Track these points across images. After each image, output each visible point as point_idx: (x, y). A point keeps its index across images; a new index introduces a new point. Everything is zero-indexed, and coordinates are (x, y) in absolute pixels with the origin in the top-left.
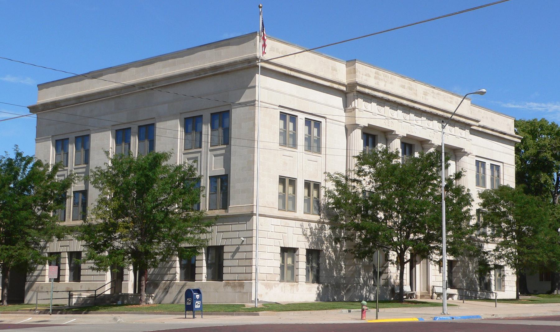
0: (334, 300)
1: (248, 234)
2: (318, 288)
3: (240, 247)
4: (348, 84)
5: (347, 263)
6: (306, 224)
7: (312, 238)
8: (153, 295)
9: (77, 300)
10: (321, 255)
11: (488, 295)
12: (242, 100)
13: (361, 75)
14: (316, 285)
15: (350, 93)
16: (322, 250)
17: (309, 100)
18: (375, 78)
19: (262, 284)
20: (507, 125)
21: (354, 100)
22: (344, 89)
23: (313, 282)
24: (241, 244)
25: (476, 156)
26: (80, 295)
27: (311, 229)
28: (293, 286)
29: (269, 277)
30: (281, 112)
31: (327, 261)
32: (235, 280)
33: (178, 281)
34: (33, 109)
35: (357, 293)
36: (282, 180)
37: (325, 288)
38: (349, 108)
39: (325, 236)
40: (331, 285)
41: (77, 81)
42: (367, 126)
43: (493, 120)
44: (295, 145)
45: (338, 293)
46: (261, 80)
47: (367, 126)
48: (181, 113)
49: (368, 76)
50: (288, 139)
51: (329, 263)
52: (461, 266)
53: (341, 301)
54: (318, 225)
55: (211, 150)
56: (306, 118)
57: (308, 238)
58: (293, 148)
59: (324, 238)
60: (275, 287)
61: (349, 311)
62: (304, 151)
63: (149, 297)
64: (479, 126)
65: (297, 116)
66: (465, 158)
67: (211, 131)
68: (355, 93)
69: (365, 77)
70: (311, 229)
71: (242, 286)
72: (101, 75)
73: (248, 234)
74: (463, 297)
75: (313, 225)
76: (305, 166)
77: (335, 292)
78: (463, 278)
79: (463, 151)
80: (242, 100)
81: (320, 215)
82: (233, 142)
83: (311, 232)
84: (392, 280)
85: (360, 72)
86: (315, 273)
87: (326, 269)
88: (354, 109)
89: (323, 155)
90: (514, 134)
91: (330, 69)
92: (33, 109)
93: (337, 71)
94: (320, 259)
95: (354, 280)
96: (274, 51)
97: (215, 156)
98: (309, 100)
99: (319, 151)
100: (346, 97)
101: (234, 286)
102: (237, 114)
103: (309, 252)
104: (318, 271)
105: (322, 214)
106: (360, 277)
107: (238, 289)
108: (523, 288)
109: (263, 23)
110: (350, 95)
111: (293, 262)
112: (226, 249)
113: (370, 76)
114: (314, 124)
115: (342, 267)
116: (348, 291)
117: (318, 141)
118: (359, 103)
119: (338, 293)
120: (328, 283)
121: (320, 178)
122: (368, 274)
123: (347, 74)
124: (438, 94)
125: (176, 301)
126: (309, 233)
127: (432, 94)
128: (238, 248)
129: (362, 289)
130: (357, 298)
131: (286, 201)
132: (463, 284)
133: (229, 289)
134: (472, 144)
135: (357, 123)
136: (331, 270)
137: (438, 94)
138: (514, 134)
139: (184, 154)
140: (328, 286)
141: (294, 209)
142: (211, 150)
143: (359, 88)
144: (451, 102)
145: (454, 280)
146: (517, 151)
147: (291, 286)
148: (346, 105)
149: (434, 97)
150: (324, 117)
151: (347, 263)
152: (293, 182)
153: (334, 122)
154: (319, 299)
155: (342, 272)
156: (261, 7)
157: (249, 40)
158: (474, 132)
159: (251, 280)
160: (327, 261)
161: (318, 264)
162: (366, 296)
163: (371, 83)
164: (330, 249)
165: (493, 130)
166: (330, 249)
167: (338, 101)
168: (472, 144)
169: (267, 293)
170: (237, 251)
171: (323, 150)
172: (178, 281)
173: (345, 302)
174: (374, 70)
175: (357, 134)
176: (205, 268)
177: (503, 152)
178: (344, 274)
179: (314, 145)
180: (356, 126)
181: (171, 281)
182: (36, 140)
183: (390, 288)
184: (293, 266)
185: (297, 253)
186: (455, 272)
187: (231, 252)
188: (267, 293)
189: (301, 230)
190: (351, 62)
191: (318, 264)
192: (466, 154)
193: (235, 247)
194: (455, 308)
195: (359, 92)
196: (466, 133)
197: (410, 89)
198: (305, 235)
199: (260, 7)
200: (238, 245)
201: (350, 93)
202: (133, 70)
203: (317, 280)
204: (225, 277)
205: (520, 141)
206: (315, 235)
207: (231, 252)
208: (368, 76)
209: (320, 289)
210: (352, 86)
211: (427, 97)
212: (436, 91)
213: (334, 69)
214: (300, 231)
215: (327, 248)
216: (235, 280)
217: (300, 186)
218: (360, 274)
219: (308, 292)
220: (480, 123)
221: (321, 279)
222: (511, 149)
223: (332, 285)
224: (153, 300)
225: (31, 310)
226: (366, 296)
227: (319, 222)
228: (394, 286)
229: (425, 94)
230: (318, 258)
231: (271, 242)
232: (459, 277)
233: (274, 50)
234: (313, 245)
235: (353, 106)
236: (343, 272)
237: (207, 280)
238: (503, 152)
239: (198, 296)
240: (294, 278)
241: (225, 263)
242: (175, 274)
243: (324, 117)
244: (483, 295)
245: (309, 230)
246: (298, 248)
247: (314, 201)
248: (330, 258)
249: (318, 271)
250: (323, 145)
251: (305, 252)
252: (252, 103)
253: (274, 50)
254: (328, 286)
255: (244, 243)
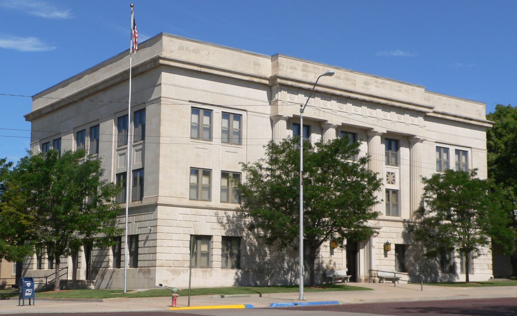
0: (256, 286)
1: (153, 223)
2: (236, 274)
3: (150, 235)
4: (271, 77)
5: (272, 249)
6: (221, 213)
7: (229, 226)
8: (95, 281)
9: (39, 286)
10: (242, 241)
11: (451, 277)
12: (153, 98)
13: (285, 69)
14: (235, 271)
15: (272, 86)
16: (242, 237)
17: (225, 95)
18: (303, 70)
19: (167, 270)
20: (478, 111)
21: (277, 93)
22: (267, 82)
23: (233, 268)
24: (150, 233)
25: (436, 142)
26: (42, 281)
27: (228, 217)
28: (206, 271)
29: (176, 264)
30: (192, 107)
31: (248, 248)
32: (145, 267)
33: (112, 268)
34: (28, 118)
35: (281, 278)
36: (195, 171)
37: (245, 274)
38: (273, 100)
39: (245, 224)
40: (252, 271)
41: (54, 91)
42: (292, 116)
43: (457, 106)
44: (210, 139)
45: (261, 278)
46: (166, 77)
47: (292, 116)
48: (115, 113)
49: (293, 68)
50: (201, 133)
51: (251, 250)
52: (413, 250)
53: (265, 285)
54: (237, 214)
55: (134, 146)
56: (222, 112)
57: (224, 226)
58: (202, 141)
59: (243, 226)
60: (183, 272)
61: (261, 296)
62: (220, 143)
63: (90, 283)
64: (434, 112)
65: (212, 110)
66: (418, 145)
67: (135, 128)
68: (278, 85)
69: (289, 70)
70: (228, 217)
71: (149, 272)
72: (68, 84)
73: (153, 223)
74: (415, 280)
75: (230, 213)
76: (220, 157)
77: (254, 276)
78: (415, 261)
79: (415, 137)
80: (153, 98)
81: (240, 203)
82: (146, 138)
83: (228, 220)
84: (324, 265)
85: (283, 66)
86: (235, 259)
87: (246, 255)
88: (277, 101)
89: (244, 146)
90: (485, 119)
91: (252, 64)
92: (28, 118)
93: (260, 66)
94: (241, 246)
95: (277, 266)
96: (183, 50)
97: (137, 151)
98: (225, 95)
99: (240, 143)
100: (271, 90)
101: (144, 273)
102: (150, 110)
103: (226, 239)
104: (239, 257)
105: (243, 203)
106: (283, 263)
107: (147, 276)
108: (499, 271)
109: (134, 21)
110: (274, 88)
111: (208, 249)
112: (140, 238)
113: (295, 69)
114: (233, 116)
115: (266, 253)
116: (272, 275)
117: (239, 133)
118: (282, 96)
119: (261, 278)
120: (249, 269)
121: (238, 169)
122: (294, 259)
123: (272, 68)
124: (383, 83)
125: (109, 287)
126: (225, 221)
127: (376, 84)
128: (148, 237)
129: (286, 273)
130: (280, 282)
131: (199, 190)
132: (415, 268)
133: (141, 275)
134: (427, 130)
135: (279, 114)
136: (253, 255)
137: (383, 83)
138: (485, 119)
139: (117, 150)
140: (248, 271)
141: (209, 199)
142: (134, 146)
143: (279, 81)
144: (399, 91)
145: (407, 264)
146: (489, 137)
147: (203, 271)
148: (271, 97)
149: (377, 86)
150: (245, 110)
151: (272, 249)
152: (207, 173)
153: (256, 114)
154: (237, 284)
155: (267, 258)
156: (133, 6)
157: (158, 41)
158: (427, 118)
159: (156, 267)
160: (248, 248)
161: (239, 251)
162: (291, 280)
163: (298, 75)
164: (251, 236)
165: (455, 116)
166: (251, 236)
167: (263, 94)
168: (427, 130)
169: (173, 279)
170: (146, 240)
171: (244, 141)
172: (112, 268)
173: (270, 286)
174: (301, 63)
175: (283, 124)
176: (128, 256)
177: (471, 138)
178: (269, 260)
179: (233, 137)
180: (279, 117)
181: (106, 268)
182: (31, 145)
183: (321, 272)
184: (208, 253)
185: (211, 240)
186: (407, 256)
187: (143, 241)
188: (173, 279)
189: (216, 218)
190: (274, 57)
191: (239, 251)
192: (418, 140)
193: (145, 236)
194: (371, 291)
195: (282, 85)
196: (420, 120)
197: (347, 79)
198: (221, 223)
199: (131, 6)
200: (148, 234)
201: (272, 86)
202: (86, 77)
203: (237, 265)
204: (140, 264)
205: (491, 126)
206: (233, 223)
207: (143, 241)
208: (293, 68)
209: (239, 274)
210: (274, 79)
211: (368, 87)
212: (380, 80)
213: (256, 64)
214: (215, 219)
215: (248, 235)
216: (145, 267)
217: (216, 177)
218: (284, 259)
219: (225, 277)
220: (434, 110)
221: (242, 265)
222: (483, 134)
223: (254, 271)
224: (95, 285)
225: (113, 292)
226: (291, 280)
227: (237, 210)
228: (326, 270)
229: (366, 83)
230: (239, 245)
231: (181, 230)
232: (411, 261)
233: (172, 48)
234: (230, 232)
235: (276, 98)
236: (268, 258)
237: (130, 267)
238: (471, 138)
239: (29, 284)
240: (209, 265)
241: (140, 251)
242: (108, 262)
243: (245, 110)
244: (445, 278)
245: (225, 218)
246: (212, 236)
247: (233, 191)
248: (251, 245)
249: (239, 257)
250: (244, 136)
251: (220, 239)
252: (158, 100)
253: (172, 48)
254: (248, 271)
255: (152, 232)
